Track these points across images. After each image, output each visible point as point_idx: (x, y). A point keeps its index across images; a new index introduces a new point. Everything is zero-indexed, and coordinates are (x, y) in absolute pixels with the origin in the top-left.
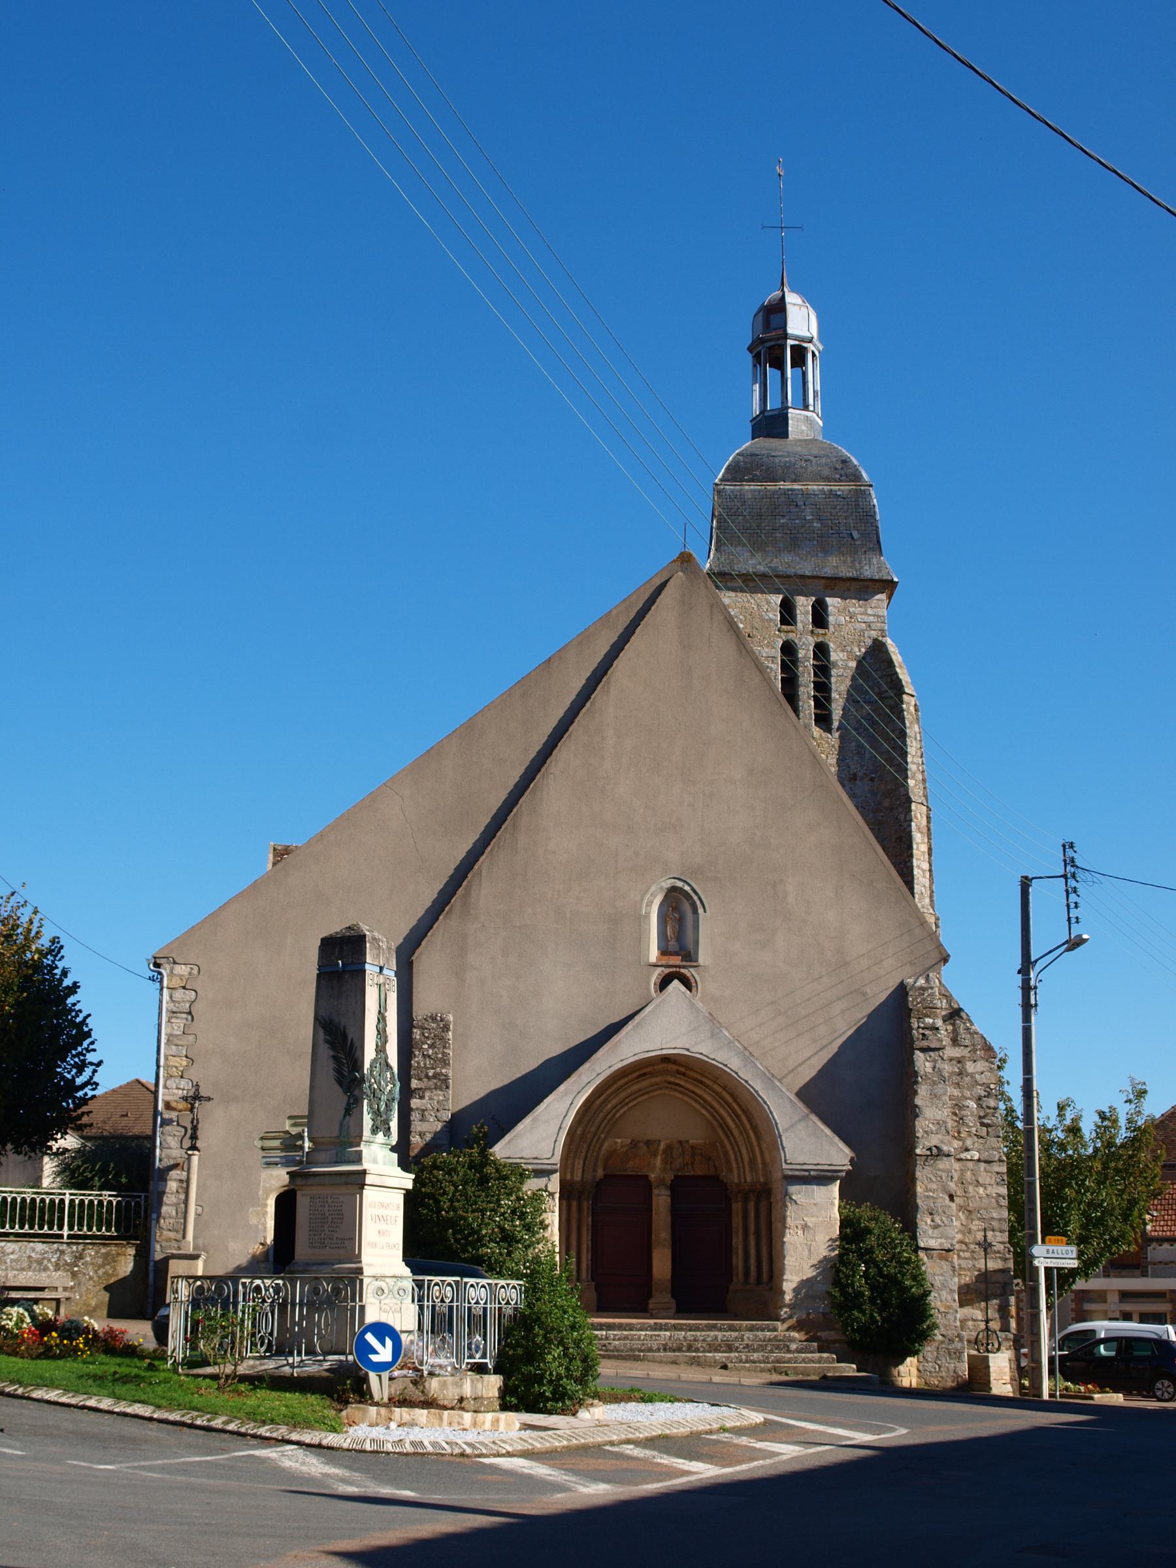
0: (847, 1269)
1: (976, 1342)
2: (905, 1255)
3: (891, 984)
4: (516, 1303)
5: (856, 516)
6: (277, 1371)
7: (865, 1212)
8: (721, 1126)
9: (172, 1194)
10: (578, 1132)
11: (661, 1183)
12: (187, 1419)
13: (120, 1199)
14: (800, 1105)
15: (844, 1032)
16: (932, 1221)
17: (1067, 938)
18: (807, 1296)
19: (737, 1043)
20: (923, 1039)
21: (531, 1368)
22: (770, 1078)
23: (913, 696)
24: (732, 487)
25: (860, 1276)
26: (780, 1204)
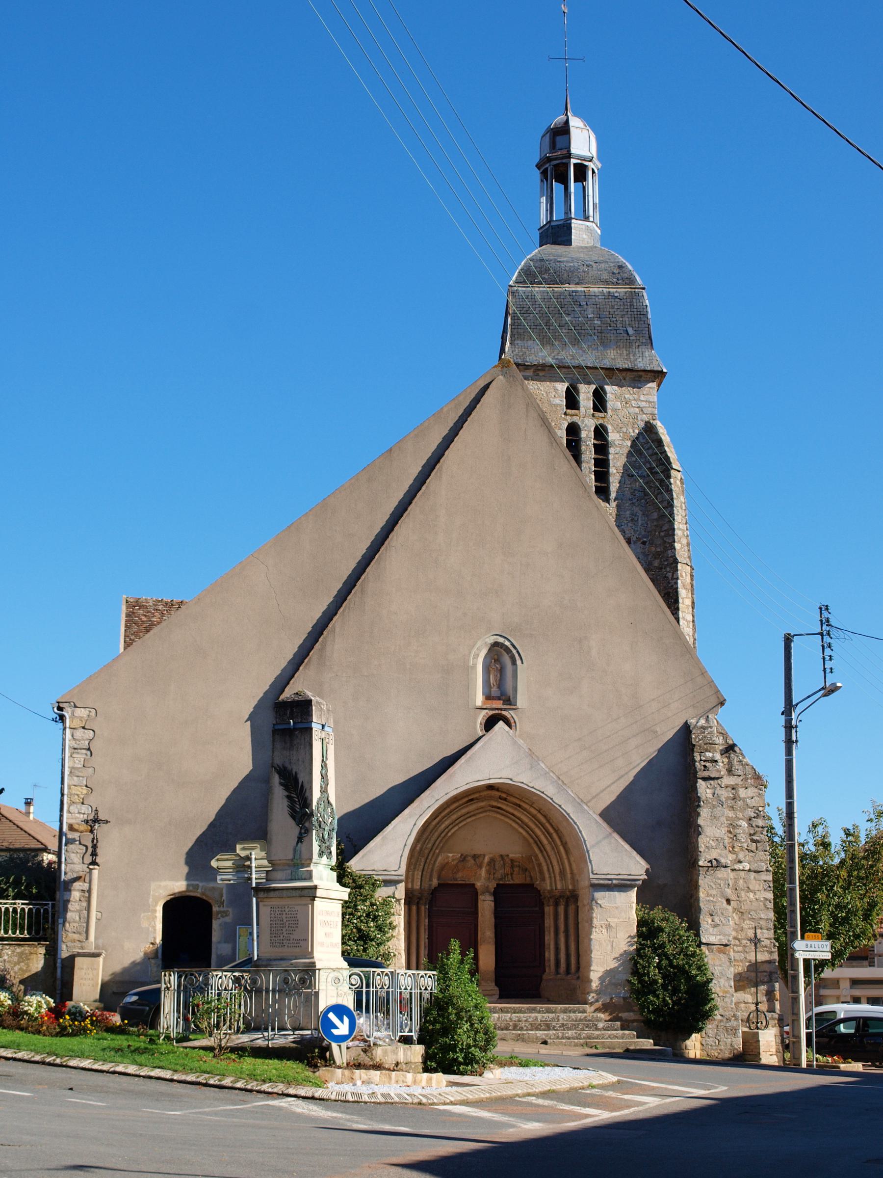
0: (643, 961)
1: (748, 1020)
2: (691, 949)
3: (677, 724)
4: (431, 990)
5: (631, 315)
6: (252, 1043)
7: (657, 914)
8: (536, 842)
9: (75, 902)
10: (418, 848)
11: (486, 890)
12: (201, 1079)
13: (31, 906)
14: (605, 825)
15: (639, 764)
16: (713, 921)
17: (823, 685)
18: (610, 983)
19: (551, 774)
20: (704, 770)
21: (447, 1040)
22: (580, 803)
23: (679, 471)
24: (524, 289)
25: (654, 967)
26: (587, 908)
